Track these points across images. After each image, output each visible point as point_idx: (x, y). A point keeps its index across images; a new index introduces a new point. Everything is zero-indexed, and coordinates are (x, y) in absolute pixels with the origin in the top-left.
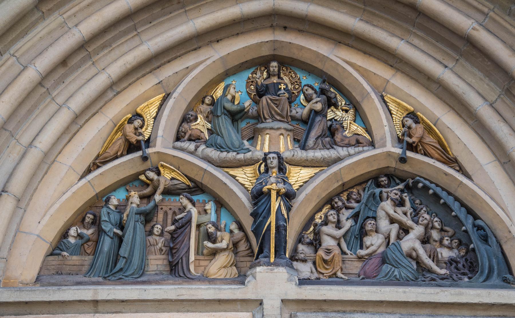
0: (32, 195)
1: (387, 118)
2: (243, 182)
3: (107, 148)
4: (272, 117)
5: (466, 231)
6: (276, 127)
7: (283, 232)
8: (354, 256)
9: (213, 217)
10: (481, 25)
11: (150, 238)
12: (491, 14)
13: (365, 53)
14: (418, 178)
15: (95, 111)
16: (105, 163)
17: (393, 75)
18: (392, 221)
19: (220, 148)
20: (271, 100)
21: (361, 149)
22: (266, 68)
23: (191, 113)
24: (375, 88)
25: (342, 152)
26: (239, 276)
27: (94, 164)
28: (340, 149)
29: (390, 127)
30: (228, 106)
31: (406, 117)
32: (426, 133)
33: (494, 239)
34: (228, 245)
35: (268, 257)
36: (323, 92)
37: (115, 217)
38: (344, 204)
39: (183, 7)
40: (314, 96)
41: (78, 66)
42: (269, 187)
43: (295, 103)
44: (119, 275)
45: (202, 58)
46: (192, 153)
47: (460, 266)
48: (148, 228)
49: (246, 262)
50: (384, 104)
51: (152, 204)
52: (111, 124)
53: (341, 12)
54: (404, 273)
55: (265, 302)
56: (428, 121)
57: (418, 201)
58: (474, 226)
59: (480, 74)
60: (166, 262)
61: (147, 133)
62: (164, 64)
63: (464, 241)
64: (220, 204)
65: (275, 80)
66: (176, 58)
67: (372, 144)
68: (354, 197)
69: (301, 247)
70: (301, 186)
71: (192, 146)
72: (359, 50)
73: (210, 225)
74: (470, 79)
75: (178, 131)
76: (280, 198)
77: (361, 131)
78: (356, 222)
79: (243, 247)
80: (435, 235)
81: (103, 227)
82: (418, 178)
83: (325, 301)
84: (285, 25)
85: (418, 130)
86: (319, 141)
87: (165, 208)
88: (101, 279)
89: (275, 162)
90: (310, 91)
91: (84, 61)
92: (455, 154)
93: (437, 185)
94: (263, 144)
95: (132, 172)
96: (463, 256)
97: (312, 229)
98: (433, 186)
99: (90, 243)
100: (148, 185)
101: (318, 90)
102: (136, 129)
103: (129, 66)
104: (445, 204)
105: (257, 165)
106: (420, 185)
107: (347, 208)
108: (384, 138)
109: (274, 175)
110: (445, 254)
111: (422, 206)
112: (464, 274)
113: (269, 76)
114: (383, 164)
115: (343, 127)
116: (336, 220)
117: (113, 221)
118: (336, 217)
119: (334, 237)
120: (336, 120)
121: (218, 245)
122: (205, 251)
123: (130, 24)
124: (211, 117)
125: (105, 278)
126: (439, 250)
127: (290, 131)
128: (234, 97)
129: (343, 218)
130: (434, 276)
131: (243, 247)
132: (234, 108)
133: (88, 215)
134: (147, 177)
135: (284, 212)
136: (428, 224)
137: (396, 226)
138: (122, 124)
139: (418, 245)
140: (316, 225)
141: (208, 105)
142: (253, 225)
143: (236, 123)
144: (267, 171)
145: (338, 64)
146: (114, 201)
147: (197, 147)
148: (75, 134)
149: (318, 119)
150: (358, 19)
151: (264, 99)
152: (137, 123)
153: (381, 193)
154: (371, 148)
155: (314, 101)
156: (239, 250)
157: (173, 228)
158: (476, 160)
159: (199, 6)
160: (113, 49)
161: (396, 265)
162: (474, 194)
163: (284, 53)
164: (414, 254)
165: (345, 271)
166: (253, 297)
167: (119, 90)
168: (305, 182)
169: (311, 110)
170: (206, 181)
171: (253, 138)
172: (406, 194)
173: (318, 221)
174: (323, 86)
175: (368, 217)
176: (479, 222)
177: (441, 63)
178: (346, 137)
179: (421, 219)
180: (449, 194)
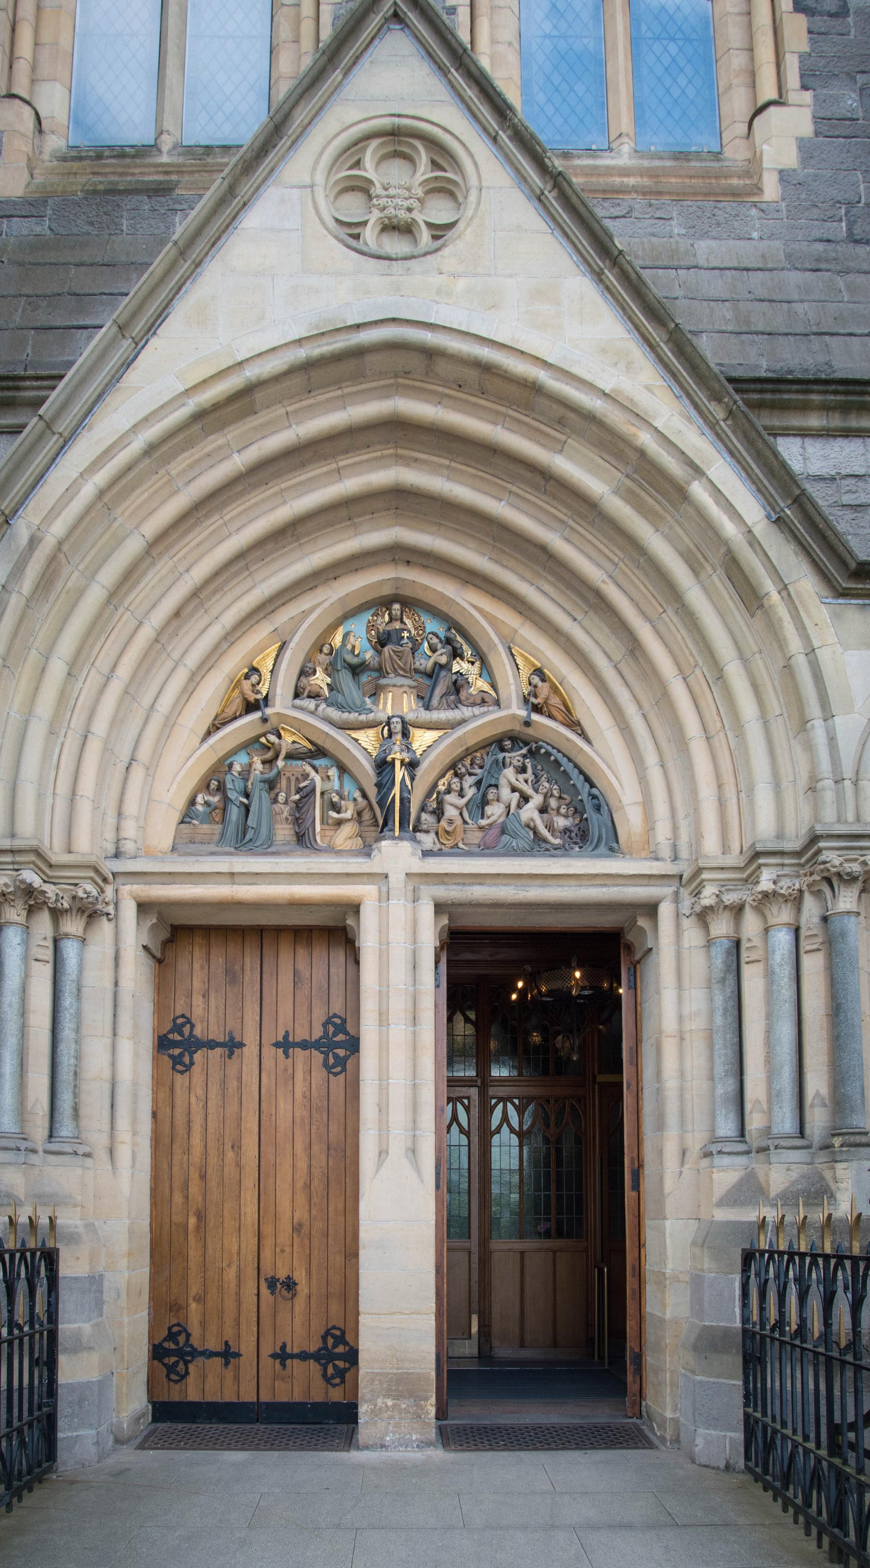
0: (158, 762)
1: (513, 675)
2: (366, 747)
3: (225, 707)
4: (395, 671)
5: (581, 801)
6: (399, 684)
7: (407, 804)
8: (475, 826)
9: (336, 785)
10: (610, 577)
11: (275, 806)
12: (621, 564)
13: (493, 596)
14: (541, 743)
15: (210, 665)
16: (225, 723)
17: (522, 624)
18: (514, 790)
19: (341, 707)
20: (394, 651)
21: (485, 709)
22: (387, 609)
23: (309, 665)
24: (502, 638)
25: (466, 712)
26: (365, 846)
27: (213, 725)
28: (464, 709)
29: (516, 685)
30: (349, 658)
31: (531, 674)
32: (552, 692)
33: (606, 808)
34: (353, 815)
35: (393, 830)
36: (448, 641)
37: (239, 784)
38: (467, 770)
39: (297, 540)
40: (439, 646)
41: (191, 615)
42: (392, 756)
43: (419, 652)
44: (250, 846)
45: (319, 600)
46: (312, 713)
47: (573, 835)
48: (273, 795)
49: (372, 833)
50: (511, 657)
51: (275, 771)
52: (227, 680)
53: (469, 548)
54: (522, 844)
55: (390, 875)
56: (554, 680)
57: (539, 767)
58: (590, 794)
59: (607, 630)
60: (292, 832)
61: (264, 689)
62: (279, 607)
63: (579, 808)
64: (343, 769)
65: (397, 625)
66: (291, 600)
67: (497, 703)
68: (478, 762)
69: (424, 816)
70: (424, 751)
71: (311, 704)
72: (487, 592)
73: (334, 794)
74: (597, 635)
75: (296, 686)
76: (403, 767)
77: (486, 687)
78: (479, 789)
79: (367, 816)
80: (553, 803)
81: (229, 795)
82: (541, 743)
83: (446, 874)
84: (409, 559)
85: (544, 689)
86: (444, 700)
87: (288, 774)
88: (232, 850)
89: (399, 727)
90: (435, 640)
91: (196, 609)
92: (578, 716)
93: (559, 751)
94: (385, 703)
95: (253, 734)
96: (577, 825)
97: (435, 796)
98: (554, 752)
99: (217, 811)
100: (269, 748)
101: (443, 638)
102: (253, 685)
103: (243, 614)
104: (564, 771)
105: (380, 728)
106: (543, 751)
107: (471, 774)
108: (509, 698)
109: (398, 743)
110: (561, 822)
111: (543, 773)
112: (576, 843)
113: (391, 620)
114: (506, 727)
115: (469, 683)
116: (458, 789)
117: (238, 788)
118: (459, 785)
119: (456, 807)
120: (461, 674)
121: (342, 816)
122: (330, 821)
123: (242, 564)
124: (330, 669)
125: (236, 848)
126: (555, 819)
127: (414, 687)
128: (354, 647)
129: (466, 785)
130: (548, 846)
131: (367, 816)
132: (355, 661)
133: (213, 782)
134: (268, 741)
135: (408, 782)
136: (547, 793)
137: (517, 794)
138: (239, 681)
139: (536, 815)
140: (439, 793)
141: (327, 655)
142: (377, 795)
143: (356, 677)
144: (390, 735)
145: (464, 609)
146: (237, 768)
147: (317, 706)
148: (192, 693)
149: (443, 673)
150: (487, 557)
151: (386, 649)
152: (254, 678)
153: (504, 758)
154: (496, 708)
155: (439, 653)
156: (363, 819)
157: (297, 797)
158: (597, 724)
159: (314, 538)
160: (226, 593)
161: (515, 835)
162: (593, 762)
163: (407, 592)
164: (532, 824)
165: (466, 841)
166: (379, 871)
167: (233, 640)
168: (429, 747)
169: (436, 663)
170: (328, 746)
171: (375, 694)
172: (528, 760)
173: (441, 788)
174: (449, 634)
175: (490, 786)
176: (594, 791)
177: (570, 615)
178: (471, 695)
179: (541, 787)
180: (570, 760)
